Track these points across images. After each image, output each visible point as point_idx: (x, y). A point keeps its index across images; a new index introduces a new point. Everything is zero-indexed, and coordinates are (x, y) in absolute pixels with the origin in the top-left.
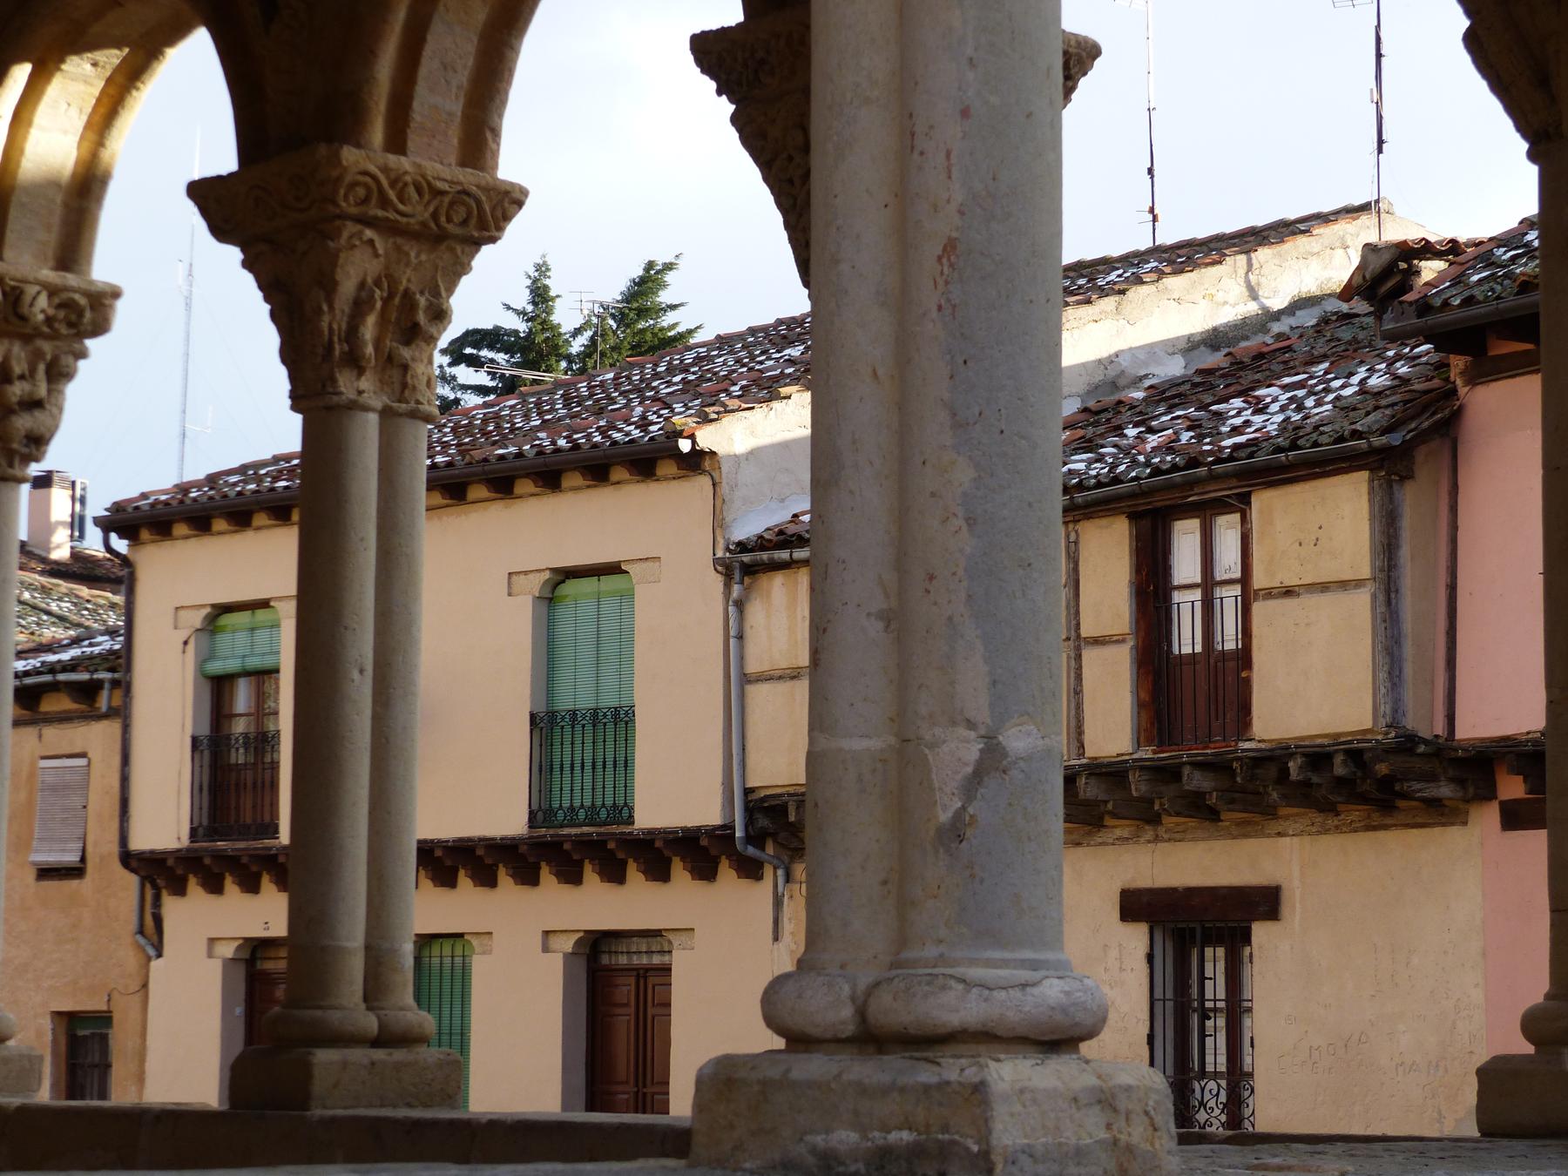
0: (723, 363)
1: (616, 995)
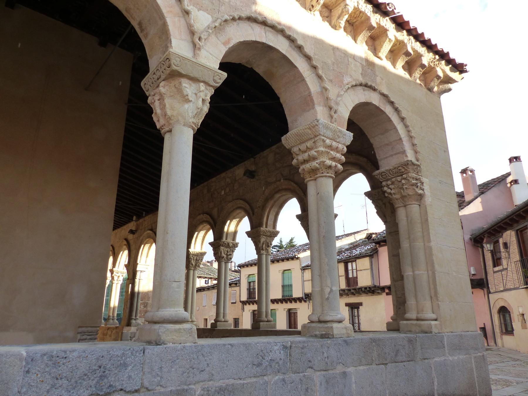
0: (300, 248)
1: (292, 316)
